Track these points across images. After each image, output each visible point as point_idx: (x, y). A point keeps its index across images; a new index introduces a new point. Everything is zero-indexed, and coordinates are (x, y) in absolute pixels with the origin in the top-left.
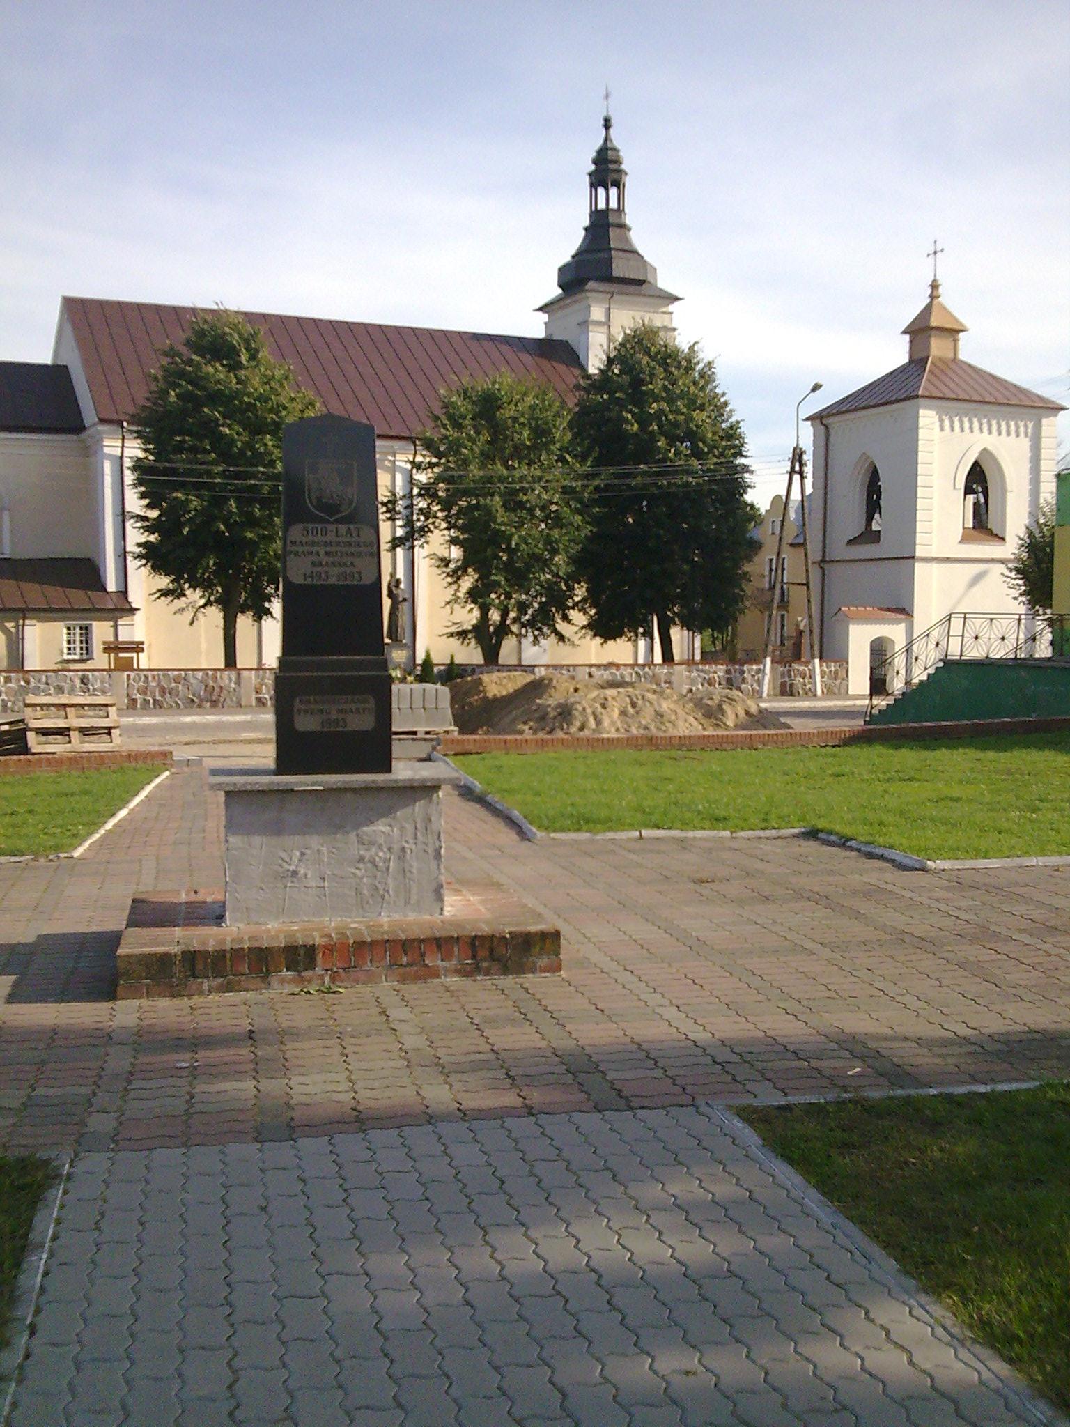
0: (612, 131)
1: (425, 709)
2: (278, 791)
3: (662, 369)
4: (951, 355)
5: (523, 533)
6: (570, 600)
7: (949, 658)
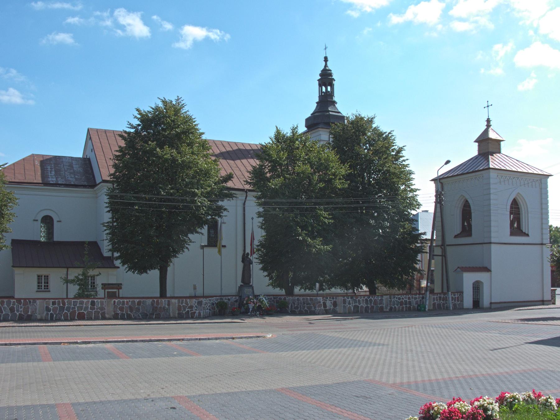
0: (328, 63)
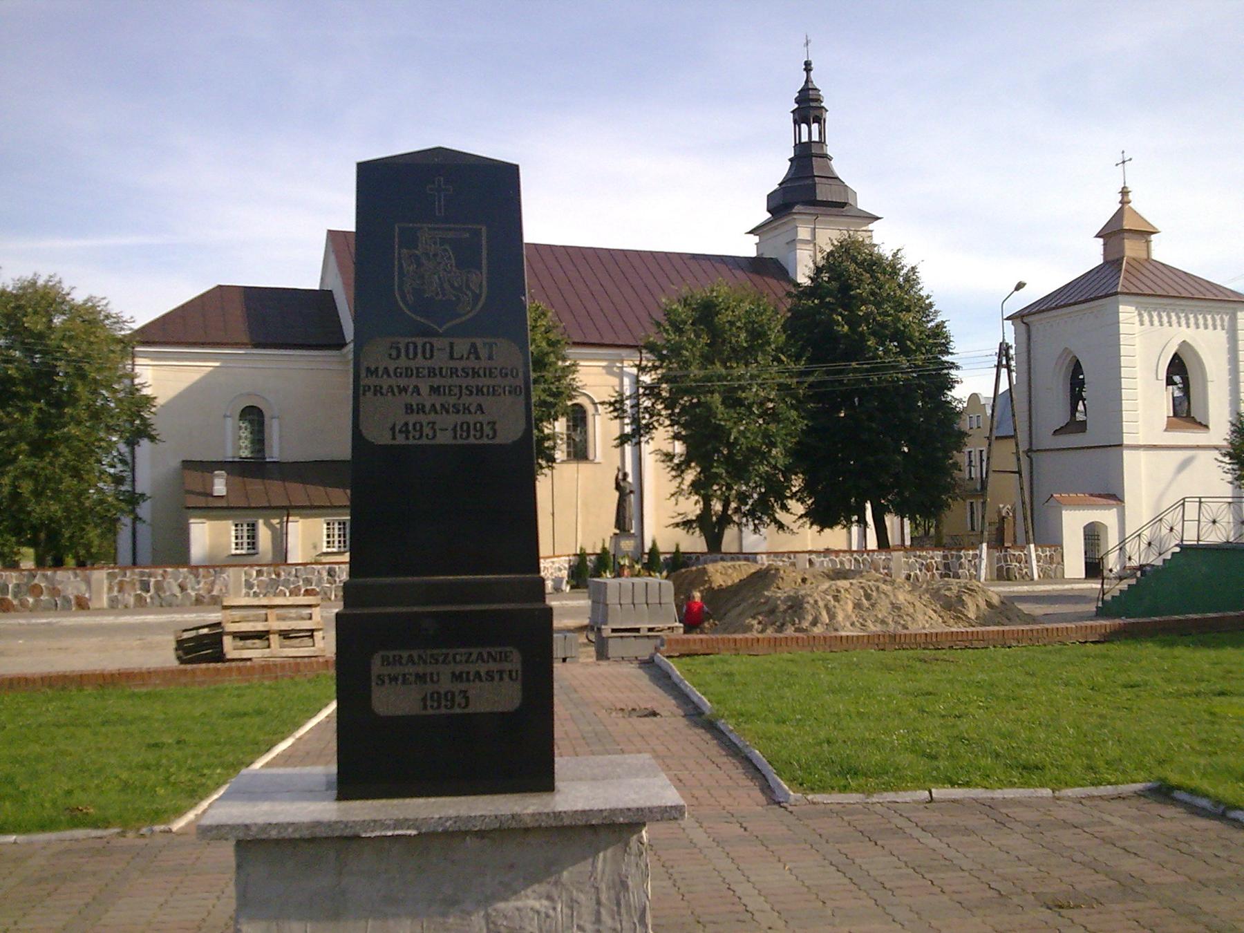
1: (647, 604)
2: (327, 838)
3: (868, 275)
4: (1146, 257)
5: (742, 428)
6: (788, 491)
7: (1185, 543)
